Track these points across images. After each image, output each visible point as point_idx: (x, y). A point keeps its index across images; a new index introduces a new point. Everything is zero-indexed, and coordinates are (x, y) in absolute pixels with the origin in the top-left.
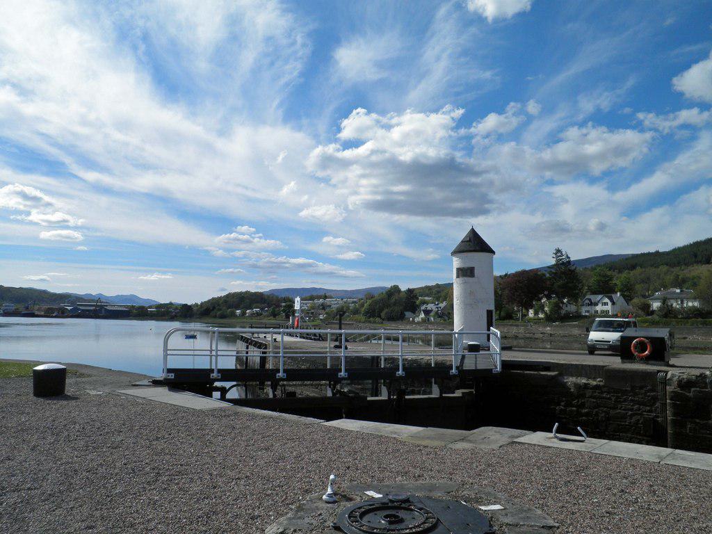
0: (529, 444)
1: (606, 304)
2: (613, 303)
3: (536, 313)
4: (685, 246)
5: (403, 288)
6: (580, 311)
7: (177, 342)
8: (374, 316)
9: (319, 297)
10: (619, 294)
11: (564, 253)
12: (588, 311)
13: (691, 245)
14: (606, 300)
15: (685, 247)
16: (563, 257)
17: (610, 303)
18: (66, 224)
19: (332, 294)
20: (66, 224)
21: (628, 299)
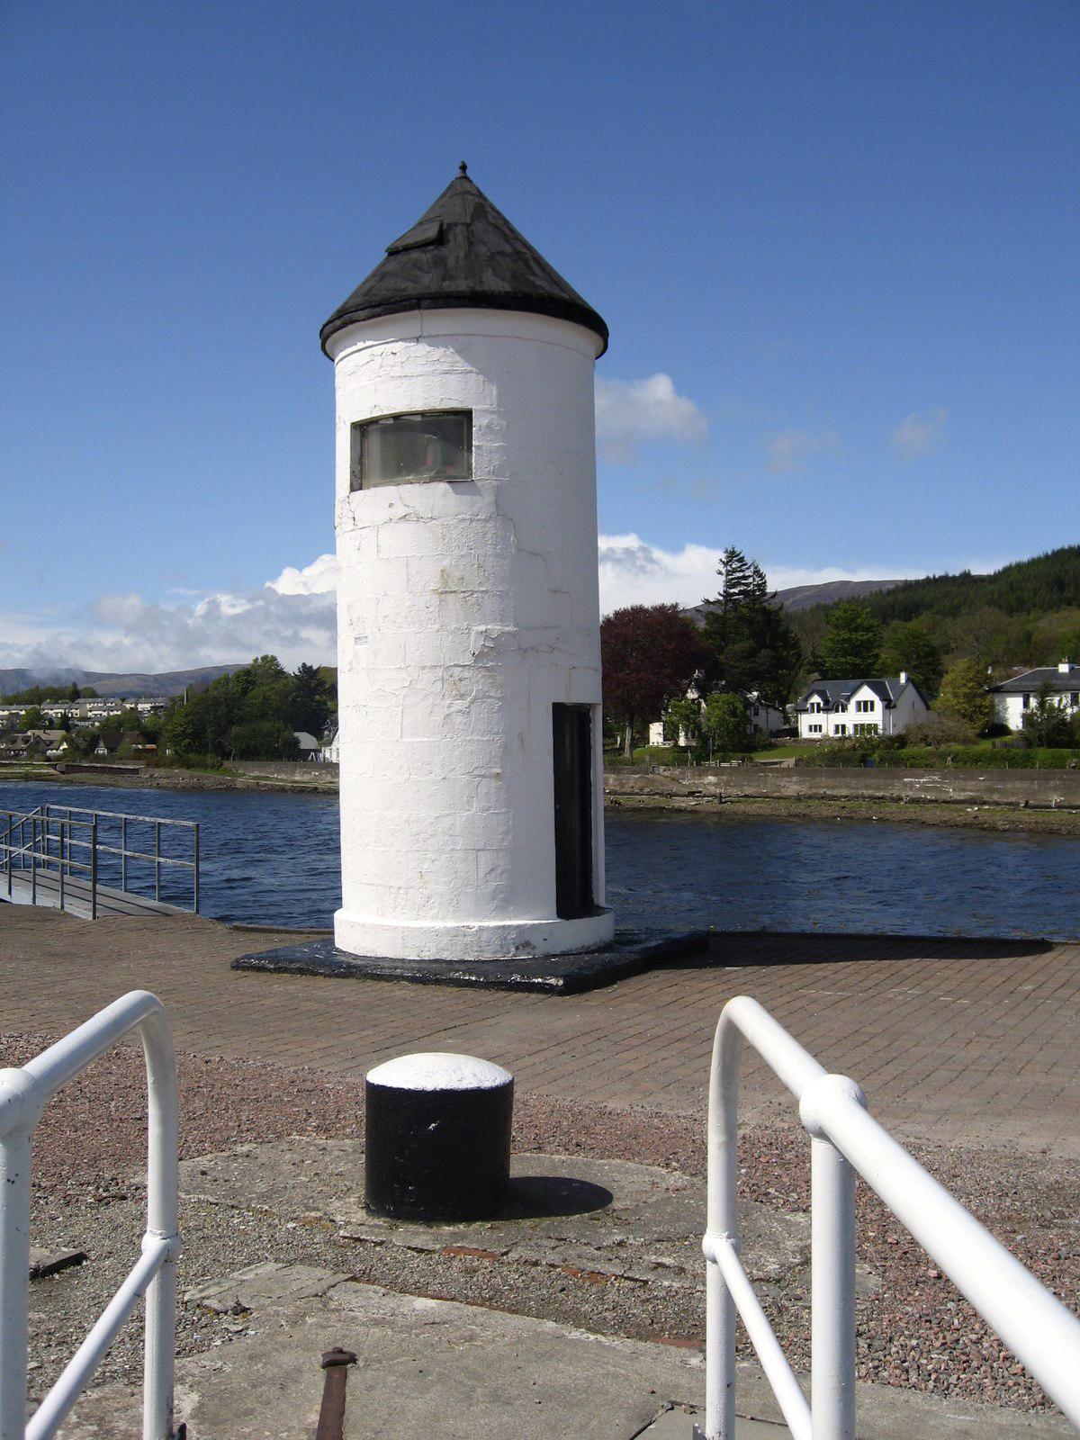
0: (315, 974)
1: (866, 706)
2: (889, 705)
3: (670, 734)
4: (1033, 560)
5: (291, 665)
6: (946, 659)
7: (682, 1033)
8: (202, 749)
9: (57, 695)
10: (903, 677)
11: (748, 560)
12: (817, 728)
13: (1047, 557)
14: (866, 693)
15: (1034, 563)
16: (748, 573)
17: (879, 705)
18: (258, 945)
19: (99, 688)
20: (258, 945)
21: (926, 688)
